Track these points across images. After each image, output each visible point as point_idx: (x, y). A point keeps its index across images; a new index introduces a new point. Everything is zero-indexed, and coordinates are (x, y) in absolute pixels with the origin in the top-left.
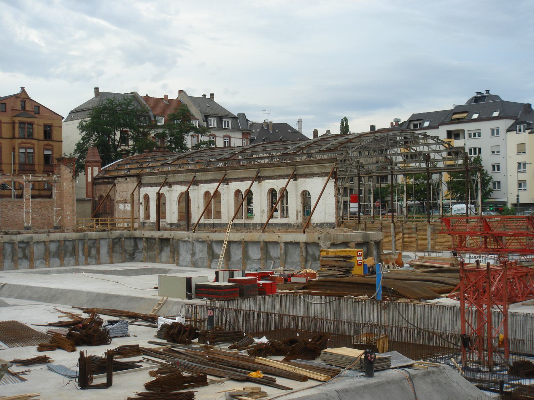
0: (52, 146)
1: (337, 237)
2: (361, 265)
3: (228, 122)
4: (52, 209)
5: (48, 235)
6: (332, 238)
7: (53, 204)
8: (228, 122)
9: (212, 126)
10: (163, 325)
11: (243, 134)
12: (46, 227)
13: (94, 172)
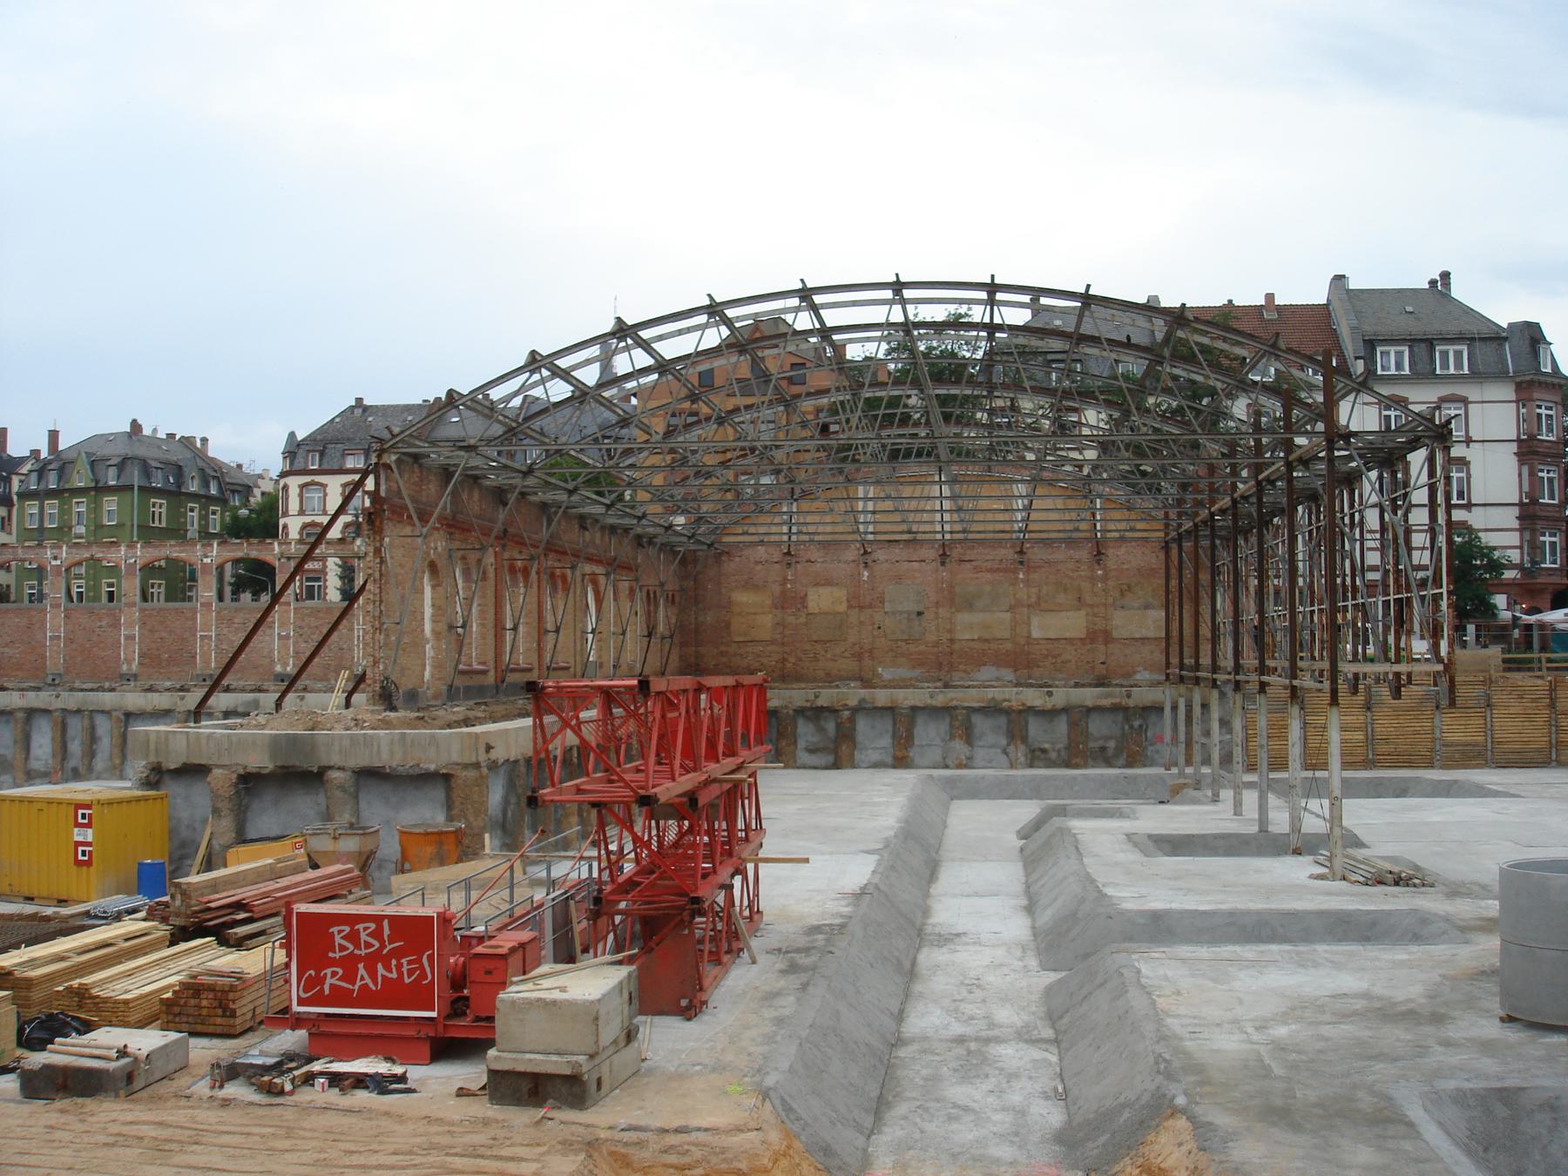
1: (167, 739)
2: (88, 863)
3: (1458, 354)
5: (302, 698)
6: (152, 747)
8: (1458, 354)
9: (1393, 371)
10: (1044, 967)
11: (1519, 387)
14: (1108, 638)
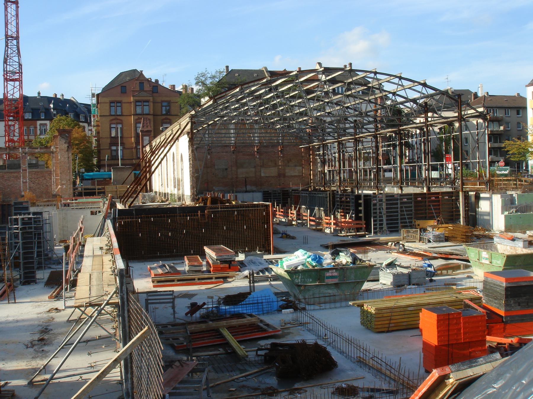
0: (121, 120)
4: (51, 179)
7: (51, 174)
12: (44, 195)
13: (144, 142)
14: (284, 176)
